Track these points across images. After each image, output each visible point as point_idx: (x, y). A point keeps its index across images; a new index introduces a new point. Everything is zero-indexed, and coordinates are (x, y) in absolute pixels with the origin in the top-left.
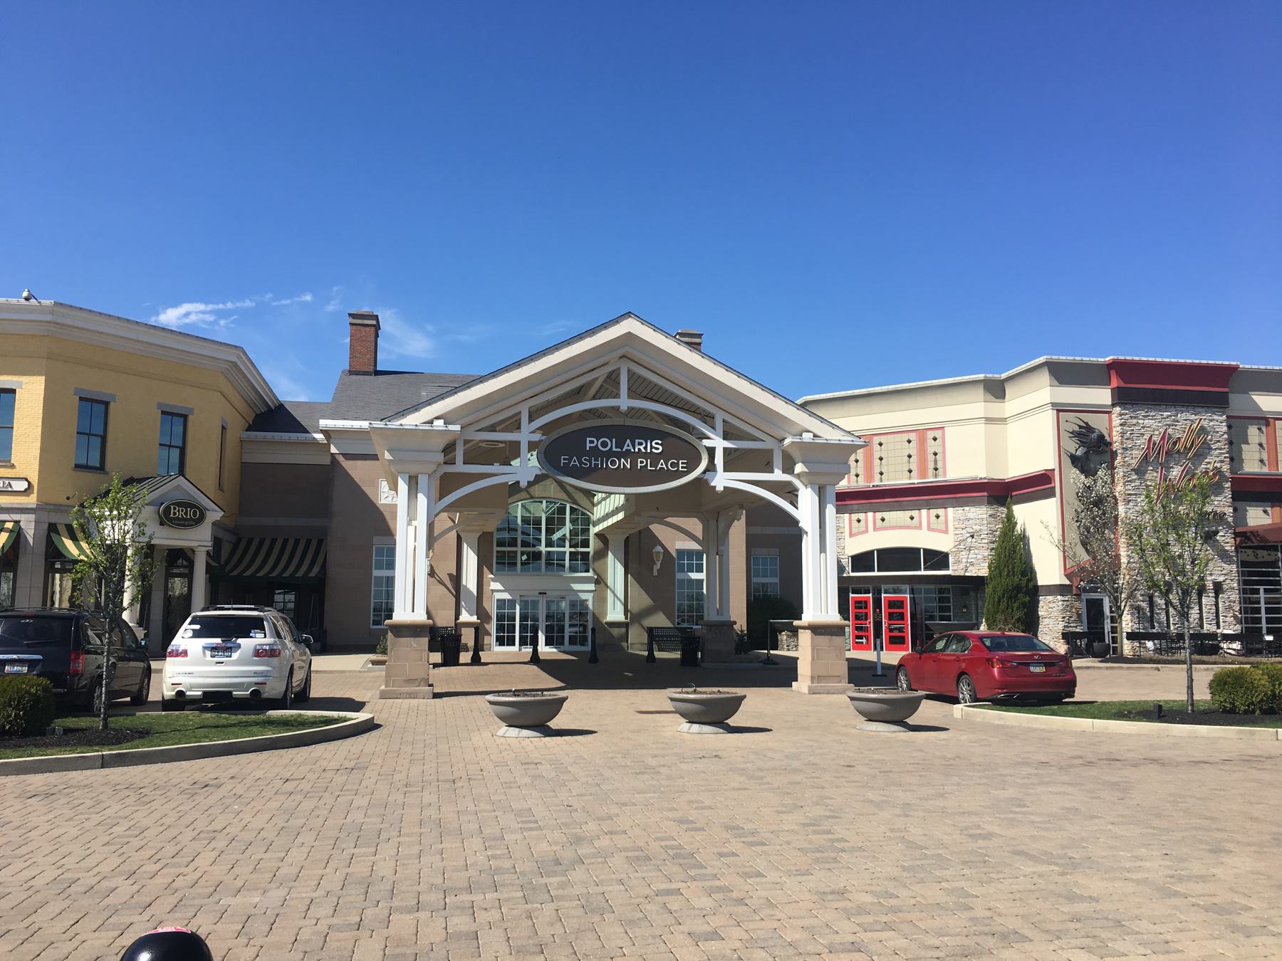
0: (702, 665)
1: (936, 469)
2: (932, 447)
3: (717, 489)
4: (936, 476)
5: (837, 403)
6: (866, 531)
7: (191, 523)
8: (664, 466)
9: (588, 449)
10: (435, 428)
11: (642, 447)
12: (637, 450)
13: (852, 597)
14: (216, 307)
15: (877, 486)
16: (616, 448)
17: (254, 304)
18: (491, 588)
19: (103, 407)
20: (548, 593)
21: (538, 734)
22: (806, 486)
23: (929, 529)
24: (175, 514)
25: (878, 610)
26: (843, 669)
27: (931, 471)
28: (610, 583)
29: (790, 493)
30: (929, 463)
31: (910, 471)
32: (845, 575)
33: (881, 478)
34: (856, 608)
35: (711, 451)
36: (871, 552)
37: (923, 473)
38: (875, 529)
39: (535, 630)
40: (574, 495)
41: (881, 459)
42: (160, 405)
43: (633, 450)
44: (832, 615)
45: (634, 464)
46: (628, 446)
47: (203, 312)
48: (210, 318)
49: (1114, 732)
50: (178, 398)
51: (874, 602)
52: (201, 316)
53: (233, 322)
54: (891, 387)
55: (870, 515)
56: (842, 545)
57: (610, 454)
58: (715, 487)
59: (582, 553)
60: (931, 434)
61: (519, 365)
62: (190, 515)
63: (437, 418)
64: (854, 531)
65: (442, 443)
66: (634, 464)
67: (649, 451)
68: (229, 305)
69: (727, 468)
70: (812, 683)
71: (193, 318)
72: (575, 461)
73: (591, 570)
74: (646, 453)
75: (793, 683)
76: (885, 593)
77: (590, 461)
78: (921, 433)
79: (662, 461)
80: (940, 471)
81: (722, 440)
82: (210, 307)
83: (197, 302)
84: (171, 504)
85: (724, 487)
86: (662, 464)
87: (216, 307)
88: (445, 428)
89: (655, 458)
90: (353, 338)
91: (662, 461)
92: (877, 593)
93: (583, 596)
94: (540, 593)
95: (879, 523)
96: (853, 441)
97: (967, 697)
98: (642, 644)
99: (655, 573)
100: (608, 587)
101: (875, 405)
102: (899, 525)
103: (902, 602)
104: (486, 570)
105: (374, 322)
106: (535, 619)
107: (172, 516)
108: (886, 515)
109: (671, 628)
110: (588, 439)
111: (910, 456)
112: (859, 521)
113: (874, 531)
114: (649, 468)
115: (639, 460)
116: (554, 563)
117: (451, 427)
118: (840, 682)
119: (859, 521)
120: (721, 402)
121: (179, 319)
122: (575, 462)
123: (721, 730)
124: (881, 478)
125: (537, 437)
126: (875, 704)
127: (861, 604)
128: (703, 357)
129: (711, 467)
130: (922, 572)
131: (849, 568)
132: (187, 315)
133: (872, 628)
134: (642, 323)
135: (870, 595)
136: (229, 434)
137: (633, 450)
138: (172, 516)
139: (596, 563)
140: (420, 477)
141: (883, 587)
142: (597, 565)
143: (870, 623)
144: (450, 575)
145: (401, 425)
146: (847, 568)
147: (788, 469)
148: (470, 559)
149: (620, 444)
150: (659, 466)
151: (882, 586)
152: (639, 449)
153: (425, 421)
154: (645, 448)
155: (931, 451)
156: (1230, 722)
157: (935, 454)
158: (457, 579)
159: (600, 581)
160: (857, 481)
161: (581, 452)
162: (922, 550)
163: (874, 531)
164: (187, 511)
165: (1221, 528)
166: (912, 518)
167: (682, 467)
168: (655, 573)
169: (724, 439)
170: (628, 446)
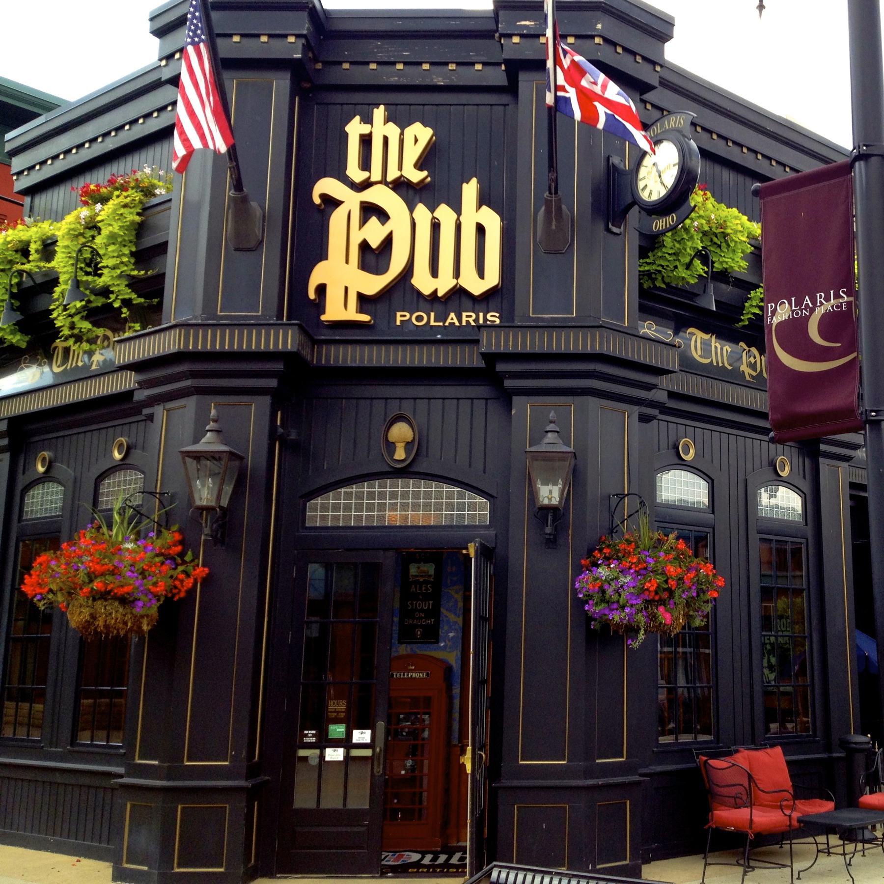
9: (398, 323)
12: (464, 323)
16: (435, 322)
152: (467, 322)
156: (637, 871)
165: (720, 578)
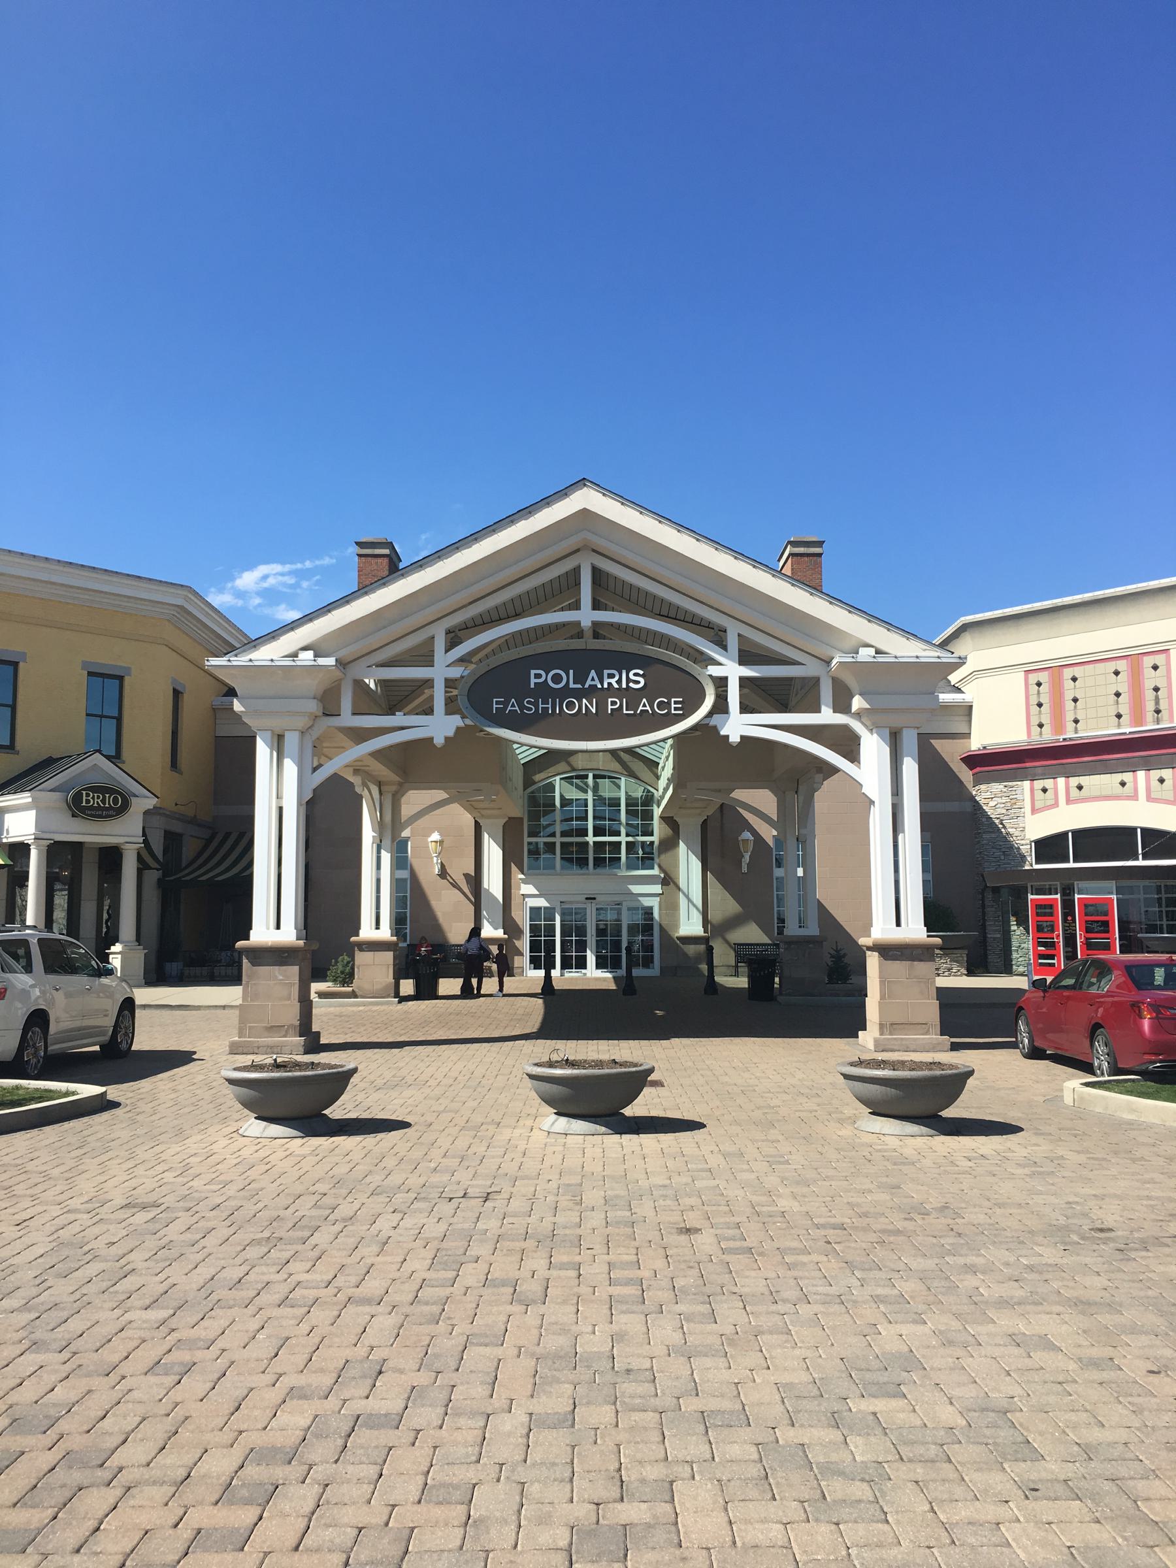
0: (780, 998)
1: (1158, 712)
2: (1151, 679)
3: (731, 740)
4: (1158, 721)
5: (1009, 623)
6: (1056, 805)
7: (111, 812)
8: (648, 708)
9: (532, 686)
10: (299, 663)
11: (613, 681)
12: (606, 686)
13: (1031, 900)
14: (294, 567)
15: (1071, 739)
16: (574, 683)
17: (335, 561)
18: (522, 892)
19: (11, 668)
20: (599, 898)
21: (294, 1133)
22: (871, 731)
23: (1149, 798)
24: (88, 801)
25: (1069, 918)
26: (931, 1011)
27: (1150, 715)
28: (682, 883)
29: (848, 745)
30: (1147, 703)
31: (1119, 716)
32: (1027, 867)
33: (1076, 728)
34: (1038, 914)
35: (721, 683)
36: (1063, 836)
37: (1138, 718)
38: (1069, 801)
39: (582, 946)
40: (629, 764)
41: (1075, 700)
42: (85, 665)
43: (599, 686)
44: (915, 930)
45: (601, 706)
46: (593, 679)
47: (282, 574)
48: (291, 580)
49: (238, 1506)
50: (108, 656)
51: (1064, 907)
52: (280, 578)
53: (318, 583)
54: (1088, 596)
55: (1061, 781)
56: (1021, 825)
57: (566, 692)
58: (727, 737)
59: (610, 843)
60: (1148, 661)
61: (421, 566)
62: (109, 804)
63: (305, 649)
64: (1038, 805)
65: (313, 685)
66: (601, 706)
67: (624, 686)
68: (308, 564)
69: (745, 709)
70: (881, 1034)
71: (271, 581)
72: (513, 706)
73: (656, 867)
74: (620, 689)
75: (860, 1033)
76: (1078, 894)
77: (536, 705)
78: (1134, 659)
79: (644, 700)
80: (1164, 714)
81: (737, 665)
82: (288, 567)
83: (273, 563)
84: (84, 789)
85: (742, 737)
86: (644, 705)
87: (294, 567)
88: (313, 663)
89: (633, 696)
90: (361, 573)
91: (644, 700)
92: (1067, 892)
93: (647, 902)
94: (587, 899)
95: (1074, 793)
96: (939, 657)
97: (1105, 1065)
98: (729, 966)
99: (745, 869)
100: (679, 889)
101: (1065, 623)
102: (1104, 793)
103: (1051, 907)
104: (514, 868)
105: (387, 551)
106: (581, 931)
107: (84, 804)
108: (1084, 780)
109: (769, 945)
110: (533, 672)
111: (1118, 695)
112: (1045, 790)
113: (1067, 804)
114: (625, 712)
115: (610, 700)
116: (606, 858)
117: (322, 661)
118: (927, 1033)
119: (1045, 790)
120: (738, 611)
121: (256, 583)
122: (513, 706)
123: (603, 1129)
124: (1076, 728)
125: (456, 672)
126: (877, 1087)
127: (1045, 909)
128: (698, 540)
129: (721, 706)
130: (1141, 862)
131: (1031, 858)
132: (265, 577)
133: (1061, 944)
134: (604, 495)
135: (1058, 896)
136: (187, 701)
137: (599, 686)
138: (84, 804)
139: (663, 857)
140: (288, 735)
141: (1077, 884)
142: (665, 858)
143: (1058, 936)
144: (466, 876)
145: (251, 660)
146: (1029, 859)
147: (842, 705)
148: (493, 854)
149: (581, 678)
150: (641, 708)
151: (1075, 883)
152: (610, 684)
153: (286, 654)
154: (619, 682)
155: (1149, 685)
157: (1156, 689)
158: (475, 880)
159: (668, 880)
160: (1041, 734)
161: (521, 690)
162: (1139, 830)
163: (1067, 804)
164: (104, 798)
166: (1123, 784)
167: (676, 709)
168: (745, 869)
169: (740, 665)
170: (593, 679)
